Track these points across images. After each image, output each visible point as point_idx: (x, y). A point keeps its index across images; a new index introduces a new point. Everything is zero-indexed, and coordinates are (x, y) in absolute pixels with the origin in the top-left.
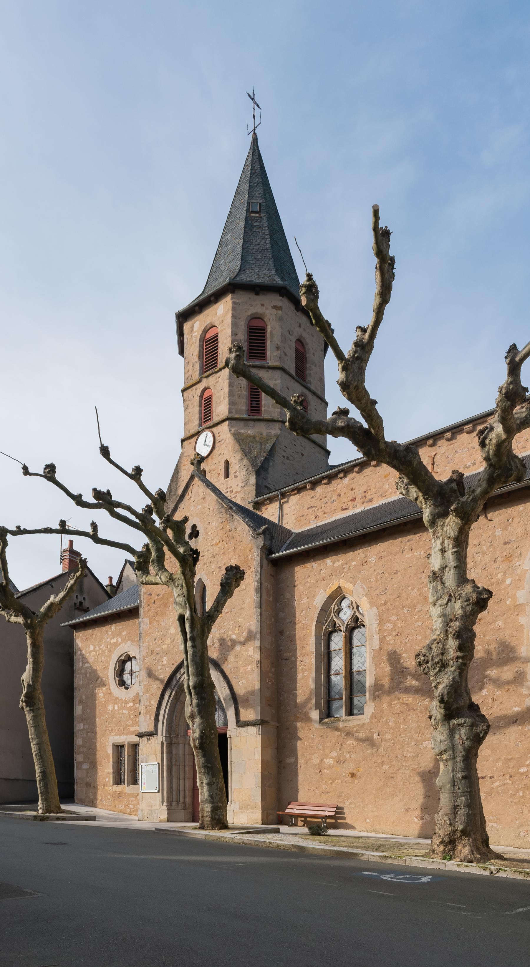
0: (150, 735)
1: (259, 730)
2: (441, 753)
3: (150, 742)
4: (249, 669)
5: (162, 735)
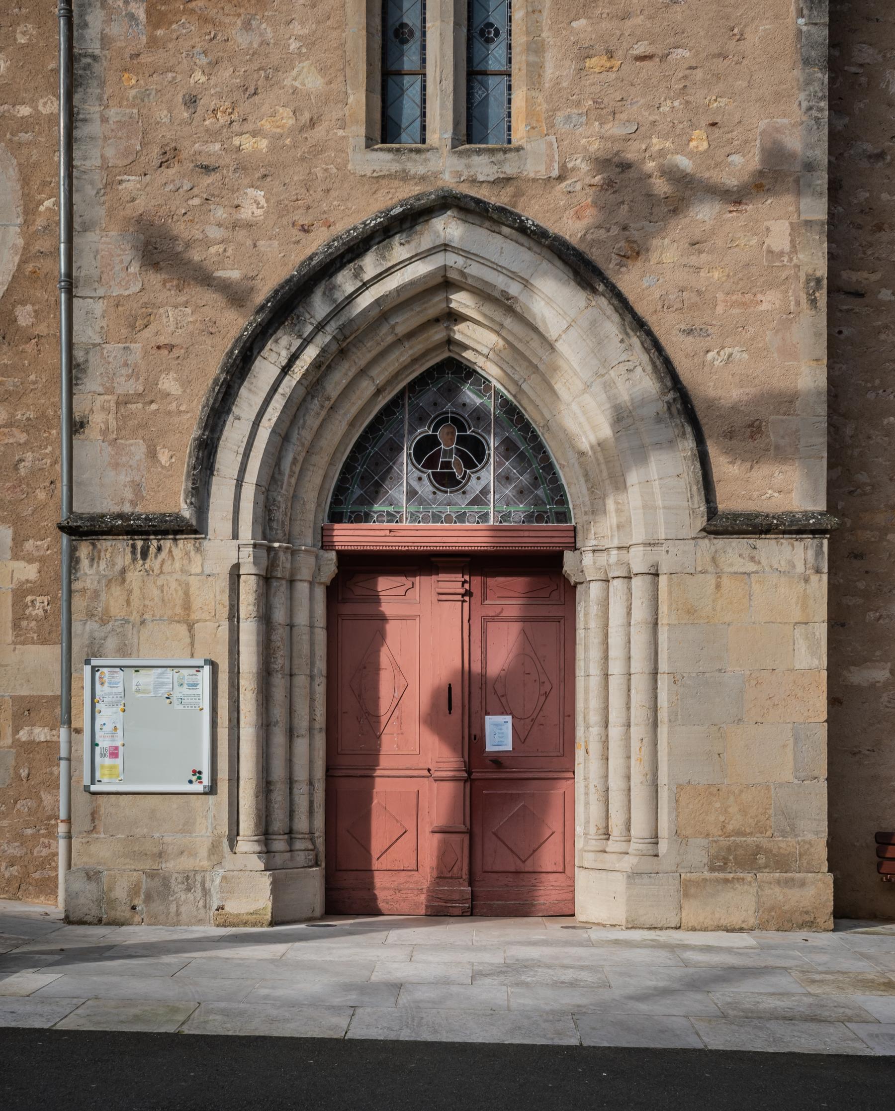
1: (819, 552)
2: (877, 661)
3: (153, 563)
4: (764, 307)
5: (235, 536)
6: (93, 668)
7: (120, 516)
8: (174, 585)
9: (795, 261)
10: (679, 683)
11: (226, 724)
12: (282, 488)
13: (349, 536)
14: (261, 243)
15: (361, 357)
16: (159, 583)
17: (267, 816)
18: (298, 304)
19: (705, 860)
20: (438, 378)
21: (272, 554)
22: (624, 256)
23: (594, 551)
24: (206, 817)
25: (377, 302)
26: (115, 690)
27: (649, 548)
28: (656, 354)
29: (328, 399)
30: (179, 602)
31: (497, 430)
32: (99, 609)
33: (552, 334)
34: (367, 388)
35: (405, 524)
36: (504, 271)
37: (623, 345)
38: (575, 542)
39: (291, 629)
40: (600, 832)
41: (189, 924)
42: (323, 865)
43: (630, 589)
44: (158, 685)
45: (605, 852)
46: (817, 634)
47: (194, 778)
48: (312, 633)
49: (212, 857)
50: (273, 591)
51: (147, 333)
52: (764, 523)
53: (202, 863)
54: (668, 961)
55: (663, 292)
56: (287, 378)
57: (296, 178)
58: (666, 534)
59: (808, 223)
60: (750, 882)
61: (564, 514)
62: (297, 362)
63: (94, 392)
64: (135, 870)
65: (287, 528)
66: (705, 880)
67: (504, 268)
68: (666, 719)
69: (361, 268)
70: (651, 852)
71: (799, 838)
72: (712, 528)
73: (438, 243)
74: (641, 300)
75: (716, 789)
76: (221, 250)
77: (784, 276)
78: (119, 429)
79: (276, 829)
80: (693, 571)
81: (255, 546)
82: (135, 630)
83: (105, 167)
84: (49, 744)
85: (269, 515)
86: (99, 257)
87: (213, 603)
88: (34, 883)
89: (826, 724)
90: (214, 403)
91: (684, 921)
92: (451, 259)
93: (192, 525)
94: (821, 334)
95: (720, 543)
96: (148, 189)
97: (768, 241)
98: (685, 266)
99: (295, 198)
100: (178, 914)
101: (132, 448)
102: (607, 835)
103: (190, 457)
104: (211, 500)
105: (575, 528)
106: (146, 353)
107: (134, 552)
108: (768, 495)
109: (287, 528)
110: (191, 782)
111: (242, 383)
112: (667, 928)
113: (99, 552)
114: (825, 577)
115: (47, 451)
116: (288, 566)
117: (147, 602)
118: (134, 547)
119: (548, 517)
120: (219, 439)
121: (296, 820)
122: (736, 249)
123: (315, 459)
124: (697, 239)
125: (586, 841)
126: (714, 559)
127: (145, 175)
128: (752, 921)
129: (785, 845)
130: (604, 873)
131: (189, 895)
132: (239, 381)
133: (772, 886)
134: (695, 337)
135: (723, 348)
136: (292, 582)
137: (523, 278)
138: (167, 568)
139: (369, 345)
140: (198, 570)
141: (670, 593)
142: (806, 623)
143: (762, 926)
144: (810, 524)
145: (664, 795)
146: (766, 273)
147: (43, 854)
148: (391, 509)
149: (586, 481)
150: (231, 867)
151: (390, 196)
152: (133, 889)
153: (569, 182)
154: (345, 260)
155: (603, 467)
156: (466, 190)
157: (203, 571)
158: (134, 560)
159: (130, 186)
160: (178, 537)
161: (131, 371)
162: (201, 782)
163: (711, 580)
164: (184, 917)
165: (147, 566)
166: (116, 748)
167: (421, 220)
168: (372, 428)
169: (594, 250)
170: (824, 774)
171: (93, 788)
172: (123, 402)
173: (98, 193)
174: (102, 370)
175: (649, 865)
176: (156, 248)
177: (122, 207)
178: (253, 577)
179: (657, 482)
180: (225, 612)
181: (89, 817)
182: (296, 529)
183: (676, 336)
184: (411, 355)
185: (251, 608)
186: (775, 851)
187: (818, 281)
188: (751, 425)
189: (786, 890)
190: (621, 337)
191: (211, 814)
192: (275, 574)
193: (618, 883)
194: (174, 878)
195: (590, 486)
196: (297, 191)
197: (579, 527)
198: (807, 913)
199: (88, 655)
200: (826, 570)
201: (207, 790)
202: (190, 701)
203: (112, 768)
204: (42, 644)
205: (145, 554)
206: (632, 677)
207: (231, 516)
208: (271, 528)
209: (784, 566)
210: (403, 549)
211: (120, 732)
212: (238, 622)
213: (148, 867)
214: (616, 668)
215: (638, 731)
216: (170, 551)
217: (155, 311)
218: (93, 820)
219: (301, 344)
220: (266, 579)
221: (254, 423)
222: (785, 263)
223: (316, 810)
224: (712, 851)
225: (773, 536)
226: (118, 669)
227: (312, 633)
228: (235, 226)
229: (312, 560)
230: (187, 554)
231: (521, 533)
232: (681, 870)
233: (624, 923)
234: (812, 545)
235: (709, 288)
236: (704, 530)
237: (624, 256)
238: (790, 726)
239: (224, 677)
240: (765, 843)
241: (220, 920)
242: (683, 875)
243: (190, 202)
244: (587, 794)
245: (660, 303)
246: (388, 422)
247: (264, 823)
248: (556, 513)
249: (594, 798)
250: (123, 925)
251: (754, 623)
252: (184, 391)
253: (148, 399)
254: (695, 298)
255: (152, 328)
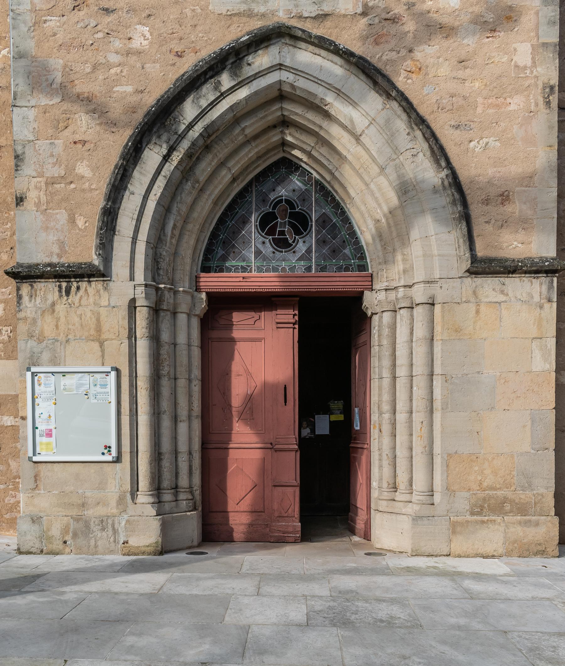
0: (70, 276)
1: (550, 287)
3: (74, 298)
4: (512, 107)
5: (132, 278)
6: (33, 373)
7: (50, 265)
8: (89, 314)
9: (535, 73)
10: (449, 381)
11: (128, 412)
12: (166, 246)
13: (214, 282)
14: (147, 66)
15: (221, 151)
16: (79, 313)
17: (159, 477)
18: (174, 110)
19: (468, 508)
20: (276, 172)
21: (160, 292)
22: (410, 72)
23: (386, 290)
24: (115, 479)
25: (231, 108)
26: (48, 389)
27: (428, 285)
28: (434, 141)
29: (198, 182)
30: (93, 326)
31: (317, 208)
32: (37, 332)
33: (357, 130)
34: (225, 176)
35: (254, 273)
36: (323, 84)
37: (409, 137)
38: (372, 285)
39: (175, 347)
40: (390, 486)
41: (104, 554)
42: (200, 509)
43: (412, 316)
44: (79, 386)
45: (394, 500)
46: (549, 346)
47: (106, 451)
48: (189, 350)
49: (119, 506)
50: (161, 319)
51: (67, 133)
52: (512, 265)
53: (112, 511)
54: (455, 592)
55: (438, 98)
56: (168, 164)
57: (171, 17)
58: (440, 275)
59: (545, 45)
60: (500, 523)
61: (364, 266)
62: (175, 153)
63: (30, 176)
64: (66, 516)
65: (170, 275)
66: (467, 522)
67: (323, 81)
68: (440, 408)
69: (219, 82)
70: (429, 502)
71: (535, 492)
72: (475, 269)
73: (274, 63)
74: (422, 103)
75: (475, 457)
76: (118, 71)
77: (527, 85)
78: (48, 203)
79: (165, 486)
80: (459, 301)
81: (146, 286)
82: (62, 347)
83: (34, 10)
84: (14, 428)
85: (157, 265)
86: (31, 77)
87: (117, 327)
88: (6, 521)
89: (554, 410)
90: (114, 181)
91: (452, 550)
92: (285, 76)
93: (100, 271)
94: (553, 127)
95: (479, 281)
96: (65, 26)
97: (515, 59)
98: (454, 78)
99: (171, 31)
100: (96, 546)
101: (58, 216)
102: (395, 488)
103: (98, 221)
104: (114, 253)
105: (372, 275)
106: (66, 147)
107: (60, 291)
108: (514, 246)
109: (170, 275)
110: (103, 454)
111: (135, 167)
112: (440, 556)
113: (36, 291)
114: (555, 305)
115: (8, 226)
116: (172, 301)
117: (70, 327)
118: (60, 287)
119: (352, 268)
120: (119, 208)
121: (180, 479)
122: (492, 65)
123: (190, 226)
124: (463, 58)
125: (381, 492)
126: (474, 292)
127: (63, 16)
128: (501, 551)
129: (525, 496)
130: (394, 516)
131: (104, 533)
132: (132, 166)
133: (515, 526)
134: (461, 131)
135: (482, 138)
136: (175, 313)
137: (336, 89)
138: (84, 302)
139: (226, 142)
140: (106, 303)
141: (443, 317)
142: (541, 338)
143: (508, 554)
144: (546, 266)
145: (438, 461)
146: (513, 83)
147: (11, 502)
148: (244, 264)
149: (380, 240)
150: (134, 514)
151: (240, 29)
152: (64, 529)
153: (369, 17)
154: (208, 76)
155: (393, 229)
156: (294, 23)
157: (109, 304)
158: (61, 296)
159: (51, 24)
160: (91, 279)
161: (55, 160)
162: (110, 454)
163: (472, 307)
164: (100, 549)
165: (69, 301)
166: (51, 430)
167: (262, 46)
168: (230, 207)
169: (388, 67)
170: (552, 446)
171: (35, 459)
172: (51, 182)
173: (29, 30)
174: (35, 160)
175: (427, 510)
176: (71, 70)
177: (47, 40)
178: (146, 308)
179: (434, 237)
180: (126, 333)
181: (33, 479)
182: (178, 276)
183: (448, 130)
184: (257, 153)
185: (144, 330)
186: (517, 501)
187: (552, 88)
188: (502, 195)
189: (525, 528)
190: (407, 131)
191: (118, 476)
192: (162, 307)
193: (405, 523)
194: (92, 521)
195: (383, 244)
196: (173, 27)
197: (374, 274)
198: (540, 544)
199: (29, 364)
200: (555, 299)
201: (115, 459)
202: (102, 396)
203: (48, 444)
204: (7, 359)
205: (68, 293)
206: (414, 378)
207: (128, 264)
208: (159, 275)
209: (525, 297)
210: (252, 291)
211: (53, 419)
212: (136, 341)
213: (75, 514)
214: (402, 372)
215: (419, 417)
216: (86, 290)
217: (72, 116)
218: (36, 481)
219: (177, 139)
220: (155, 311)
221: (144, 197)
222: (528, 74)
223: (194, 471)
224: (472, 501)
225: (518, 275)
226: (51, 374)
227: (189, 350)
228: (128, 53)
229: (189, 298)
230: (98, 291)
231: (334, 279)
232: (450, 515)
233: (409, 551)
234: (545, 281)
235: (472, 94)
236: (468, 271)
237: (410, 72)
238: (529, 412)
239: (125, 379)
240: (509, 494)
241: (126, 550)
242: (452, 518)
243: (96, 36)
244: (380, 460)
245: (436, 106)
246: (241, 203)
247: (157, 483)
248: (358, 266)
249: (386, 463)
250: (58, 554)
251: (503, 339)
252: (94, 175)
253: (68, 181)
254: (461, 102)
255: (70, 129)
